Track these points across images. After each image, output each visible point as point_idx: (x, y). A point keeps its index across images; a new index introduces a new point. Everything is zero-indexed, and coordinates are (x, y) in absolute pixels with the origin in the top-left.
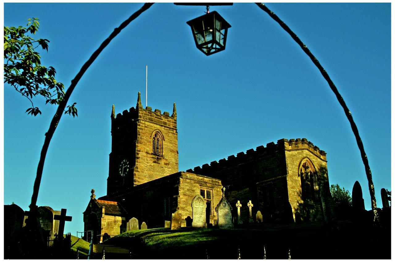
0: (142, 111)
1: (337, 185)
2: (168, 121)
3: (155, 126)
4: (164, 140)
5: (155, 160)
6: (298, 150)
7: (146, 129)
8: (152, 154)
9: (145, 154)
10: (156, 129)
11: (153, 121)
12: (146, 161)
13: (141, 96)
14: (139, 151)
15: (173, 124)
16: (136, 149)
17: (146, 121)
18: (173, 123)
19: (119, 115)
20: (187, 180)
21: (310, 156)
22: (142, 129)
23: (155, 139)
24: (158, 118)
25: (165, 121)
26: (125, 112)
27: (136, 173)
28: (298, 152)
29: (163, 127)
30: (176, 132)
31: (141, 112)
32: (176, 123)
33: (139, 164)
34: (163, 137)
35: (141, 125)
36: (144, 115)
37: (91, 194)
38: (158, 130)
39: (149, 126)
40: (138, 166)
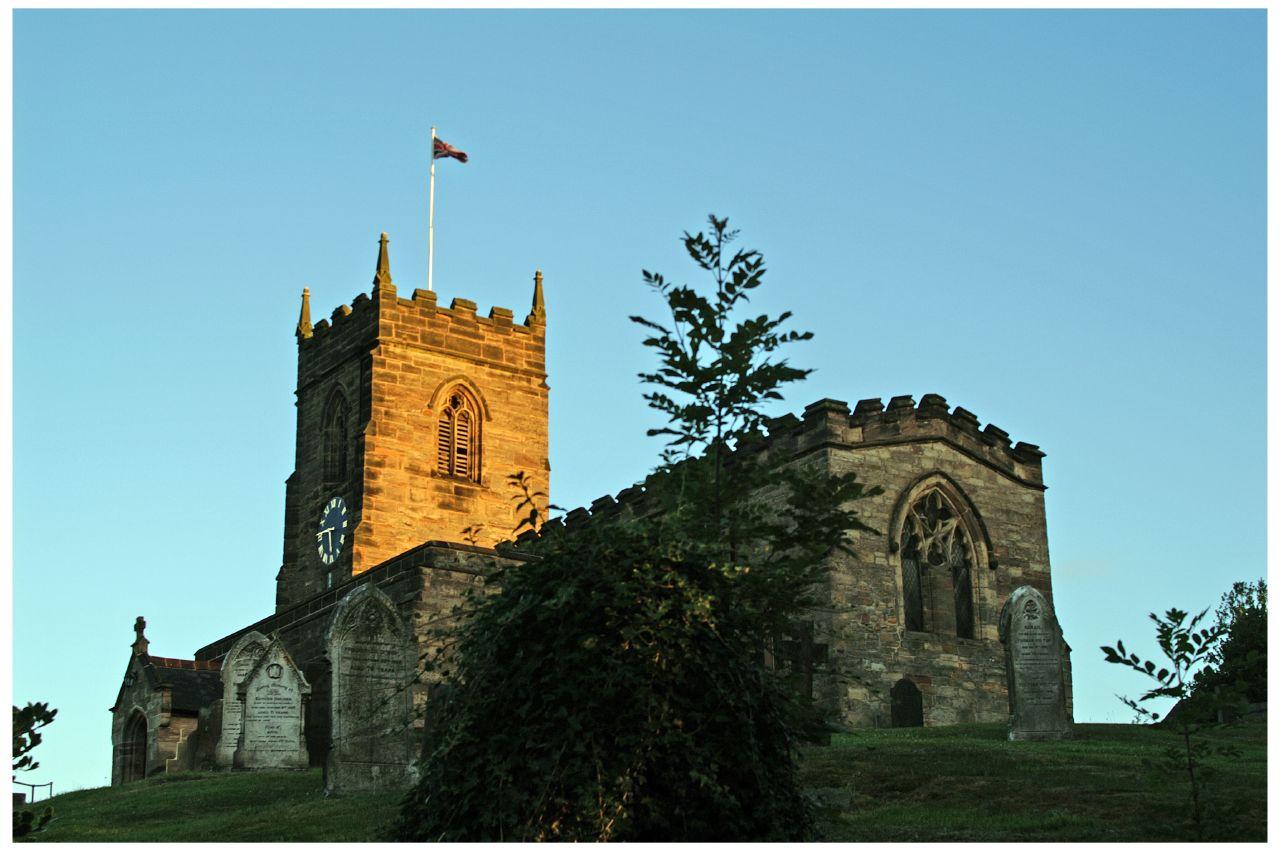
0: (393, 307)
1: (1261, 584)
2: (507, 342)
3: (450, 362)
4: (489, 419)
5: (450, 498)
6: (897, 443)
7: (409, 377)
8: (433, 474)
9: (402, 475)
10: (452, 374)
11: (439, 344)
12: (407, 501)
13: (390, 248)
14: (380, 464)
15: (529, 356)
16: (366, 457)
17: (408, 345)
18: (527, 349)
19: (322, 324)
20: (455, 575)
21: (955, 468)
22: (393, 378)
23: (449, 415)
24: (464, 333)
25: (494, 344)
26: (338, 313)
27: (361, 549)
28: (893, 453)
29: (486, 369)
30: (544, 386)
31: (388, 311)
32: (541, 350)
33: (377, 516)
34: (486, 406)
35: (389, 361)
36: (400, 323)
37: (133, 637)
38: (461, 381)
39: (423, 364)
40: (371, 525)
